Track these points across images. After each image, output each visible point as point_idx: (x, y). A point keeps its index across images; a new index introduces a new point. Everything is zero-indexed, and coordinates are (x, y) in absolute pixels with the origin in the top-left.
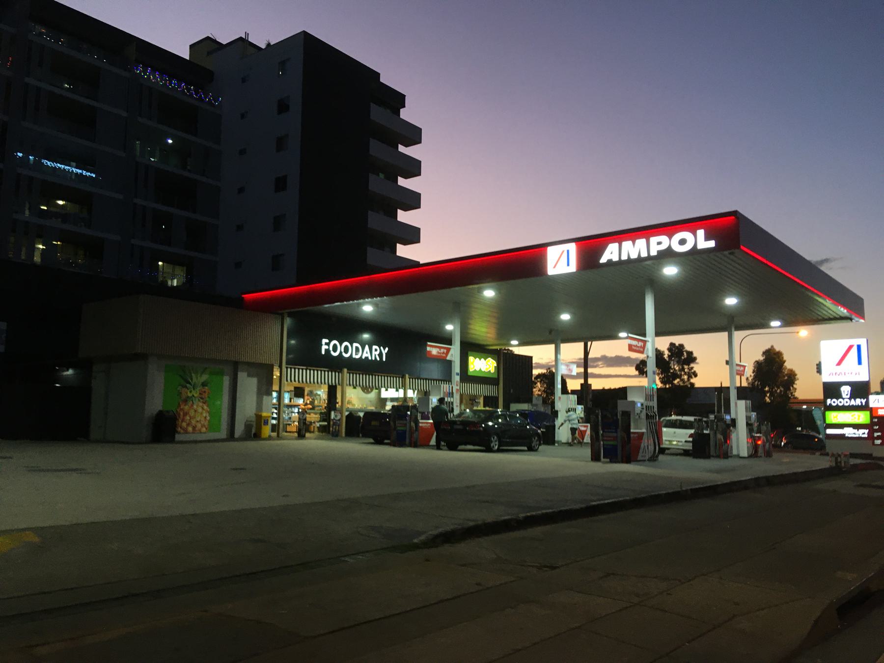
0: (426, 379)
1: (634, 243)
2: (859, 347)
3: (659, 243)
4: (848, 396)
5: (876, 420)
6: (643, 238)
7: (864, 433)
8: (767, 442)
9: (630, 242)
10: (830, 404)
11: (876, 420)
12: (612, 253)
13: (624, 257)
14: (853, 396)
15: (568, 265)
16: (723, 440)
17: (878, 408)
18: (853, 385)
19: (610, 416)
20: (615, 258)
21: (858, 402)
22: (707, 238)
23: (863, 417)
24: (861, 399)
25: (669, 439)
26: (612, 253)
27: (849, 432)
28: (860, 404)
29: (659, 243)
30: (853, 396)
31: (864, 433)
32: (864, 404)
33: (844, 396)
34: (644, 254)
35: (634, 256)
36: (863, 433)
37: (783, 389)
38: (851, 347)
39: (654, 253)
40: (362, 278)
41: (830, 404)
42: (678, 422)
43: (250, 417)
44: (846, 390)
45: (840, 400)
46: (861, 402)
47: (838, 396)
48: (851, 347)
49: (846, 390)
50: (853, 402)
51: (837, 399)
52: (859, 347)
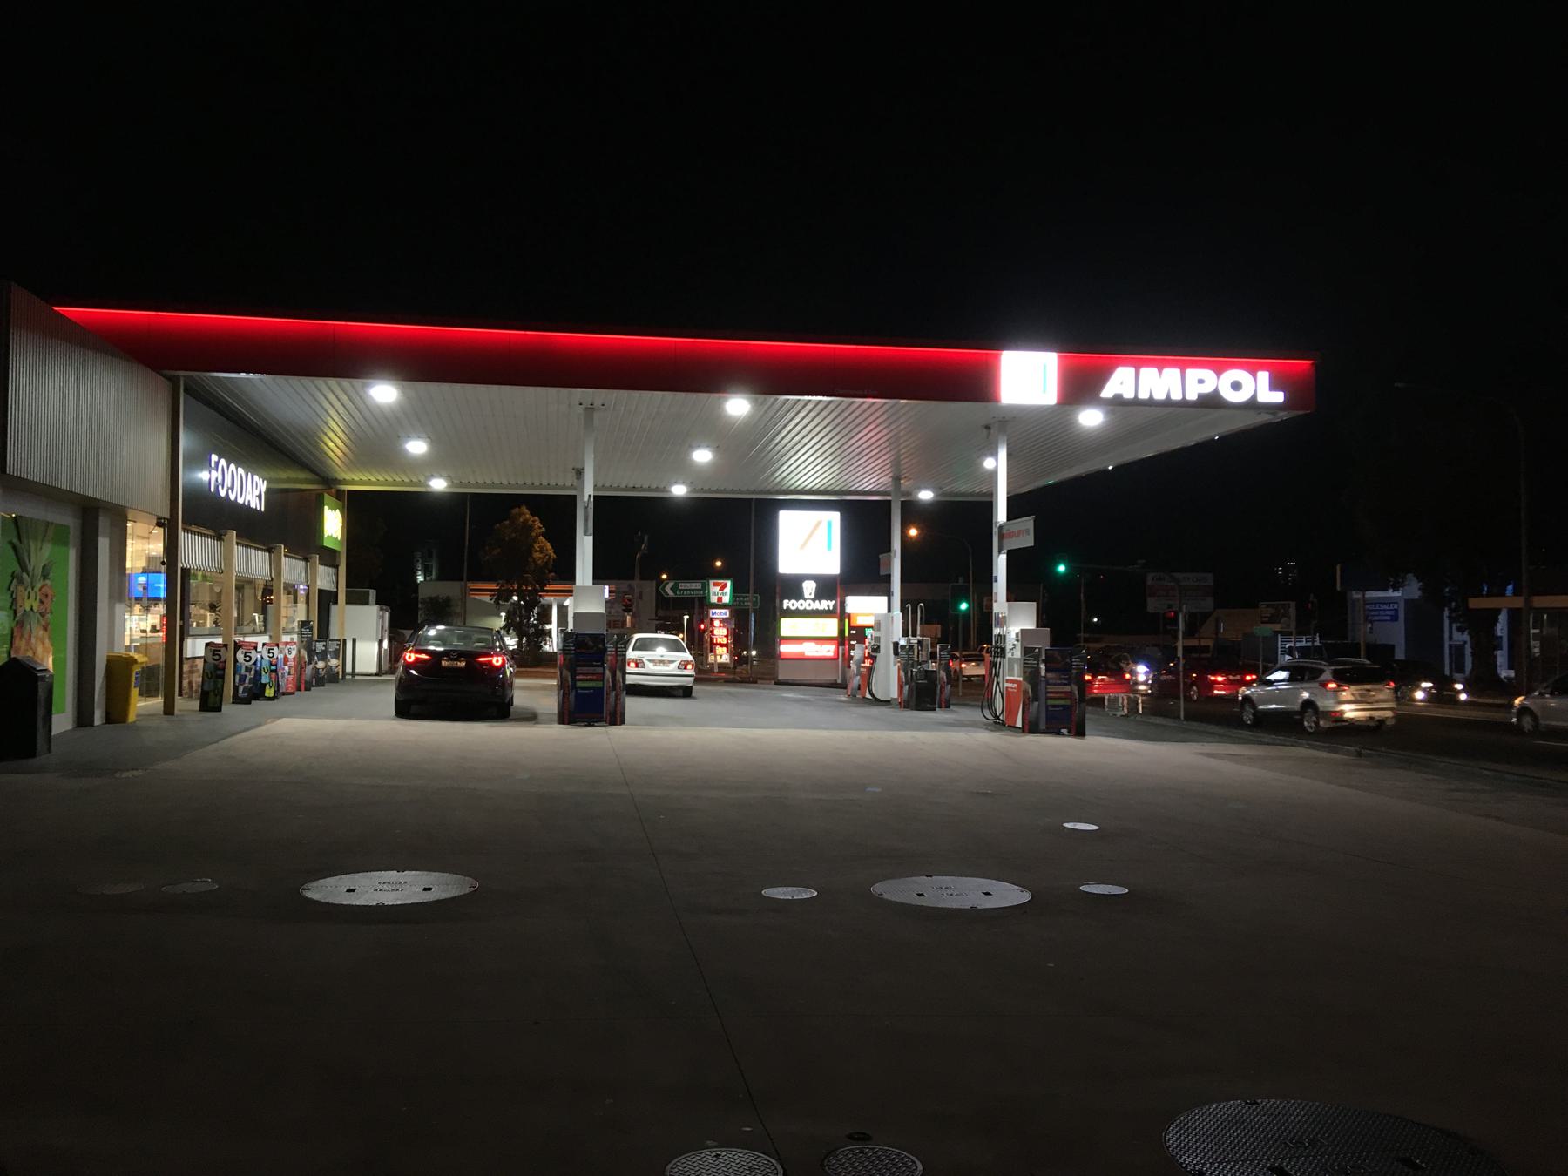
0: (191, 531)
1: (1160, 372)
2: (830, 524)
3: (1201, 381)
4: (812, 596)
5: (854, 632)
6: (1051, 351)
7: (829, 651)
8: (948, 683)
9: (1154, 371)
10: (788, 607)
11: (854, 632)
12: (1122, 383)
13: (1143, 395)
14: (819, 596)
15: (1045, 391)
16: (945, 680)
17: (858, 615)
18: (818, 579)
19: (1059, 658)
20: (1128, 394)
21: (825, 605)
22: (1274, 386)
23: (830, 627)
24: (827, 600)
25: (156, 634)
26: (1122, 383)
27: (811, 650)
28: (826, 608)
29: (1201, 381)
30: (819, 596)
31: (829, 651)
32: (831, 608)
33: (806, 595)
34: (1176, 396)
35: (1160, 396)
36: (828, 650)
37: (1466, 637)
38: (819, 523)
39: (1192, 396)
40: (343, 323)
41: (788, 607)
42: (1306, 678)
43: (8, 616)
44: (809, 588)
45: (801, 601)
46: (828, 606)
47: (798, 595)
48: (819, 523)
49: (809, 588)
50: (817, 605)
51: (797, 600)
52: (830, 524)
